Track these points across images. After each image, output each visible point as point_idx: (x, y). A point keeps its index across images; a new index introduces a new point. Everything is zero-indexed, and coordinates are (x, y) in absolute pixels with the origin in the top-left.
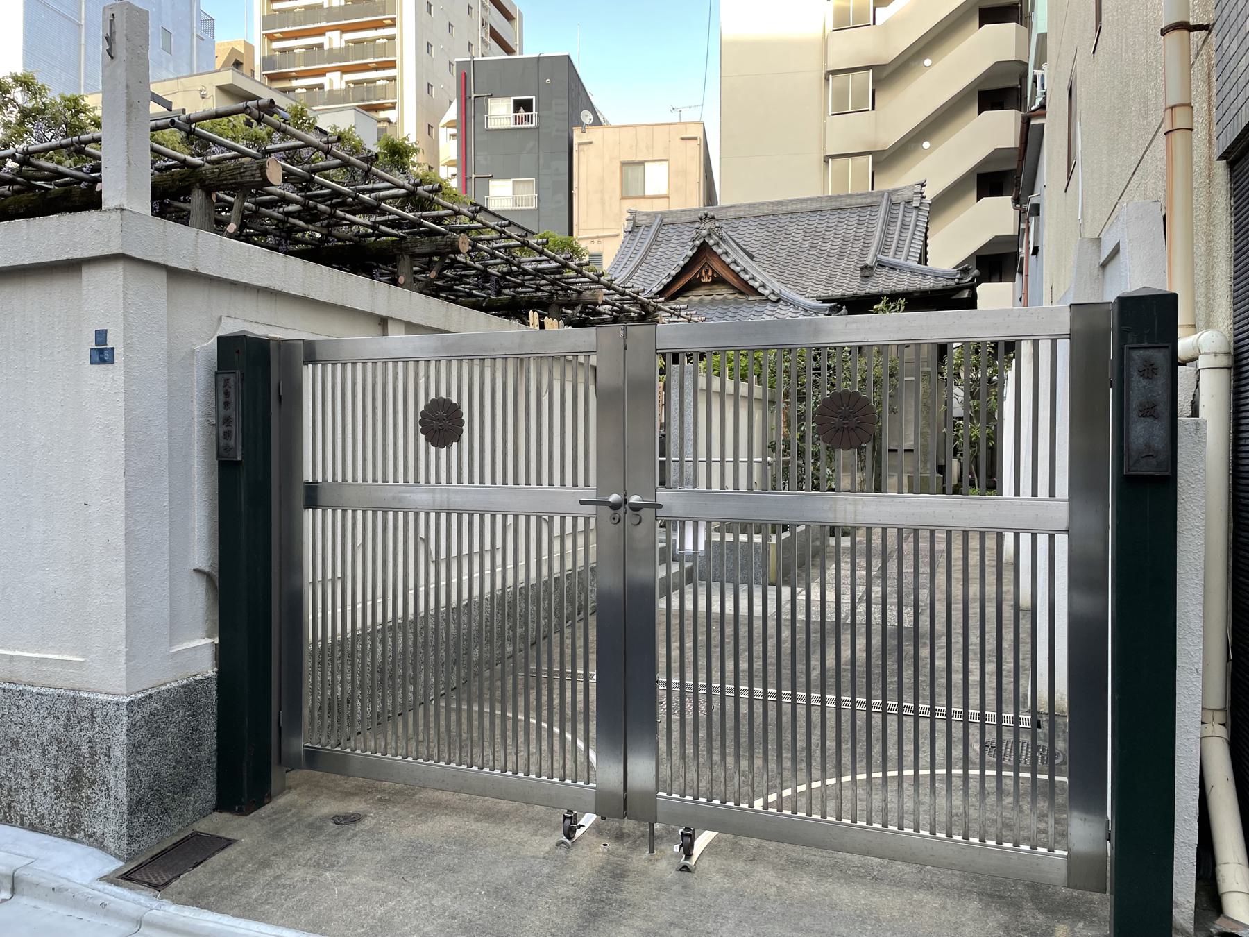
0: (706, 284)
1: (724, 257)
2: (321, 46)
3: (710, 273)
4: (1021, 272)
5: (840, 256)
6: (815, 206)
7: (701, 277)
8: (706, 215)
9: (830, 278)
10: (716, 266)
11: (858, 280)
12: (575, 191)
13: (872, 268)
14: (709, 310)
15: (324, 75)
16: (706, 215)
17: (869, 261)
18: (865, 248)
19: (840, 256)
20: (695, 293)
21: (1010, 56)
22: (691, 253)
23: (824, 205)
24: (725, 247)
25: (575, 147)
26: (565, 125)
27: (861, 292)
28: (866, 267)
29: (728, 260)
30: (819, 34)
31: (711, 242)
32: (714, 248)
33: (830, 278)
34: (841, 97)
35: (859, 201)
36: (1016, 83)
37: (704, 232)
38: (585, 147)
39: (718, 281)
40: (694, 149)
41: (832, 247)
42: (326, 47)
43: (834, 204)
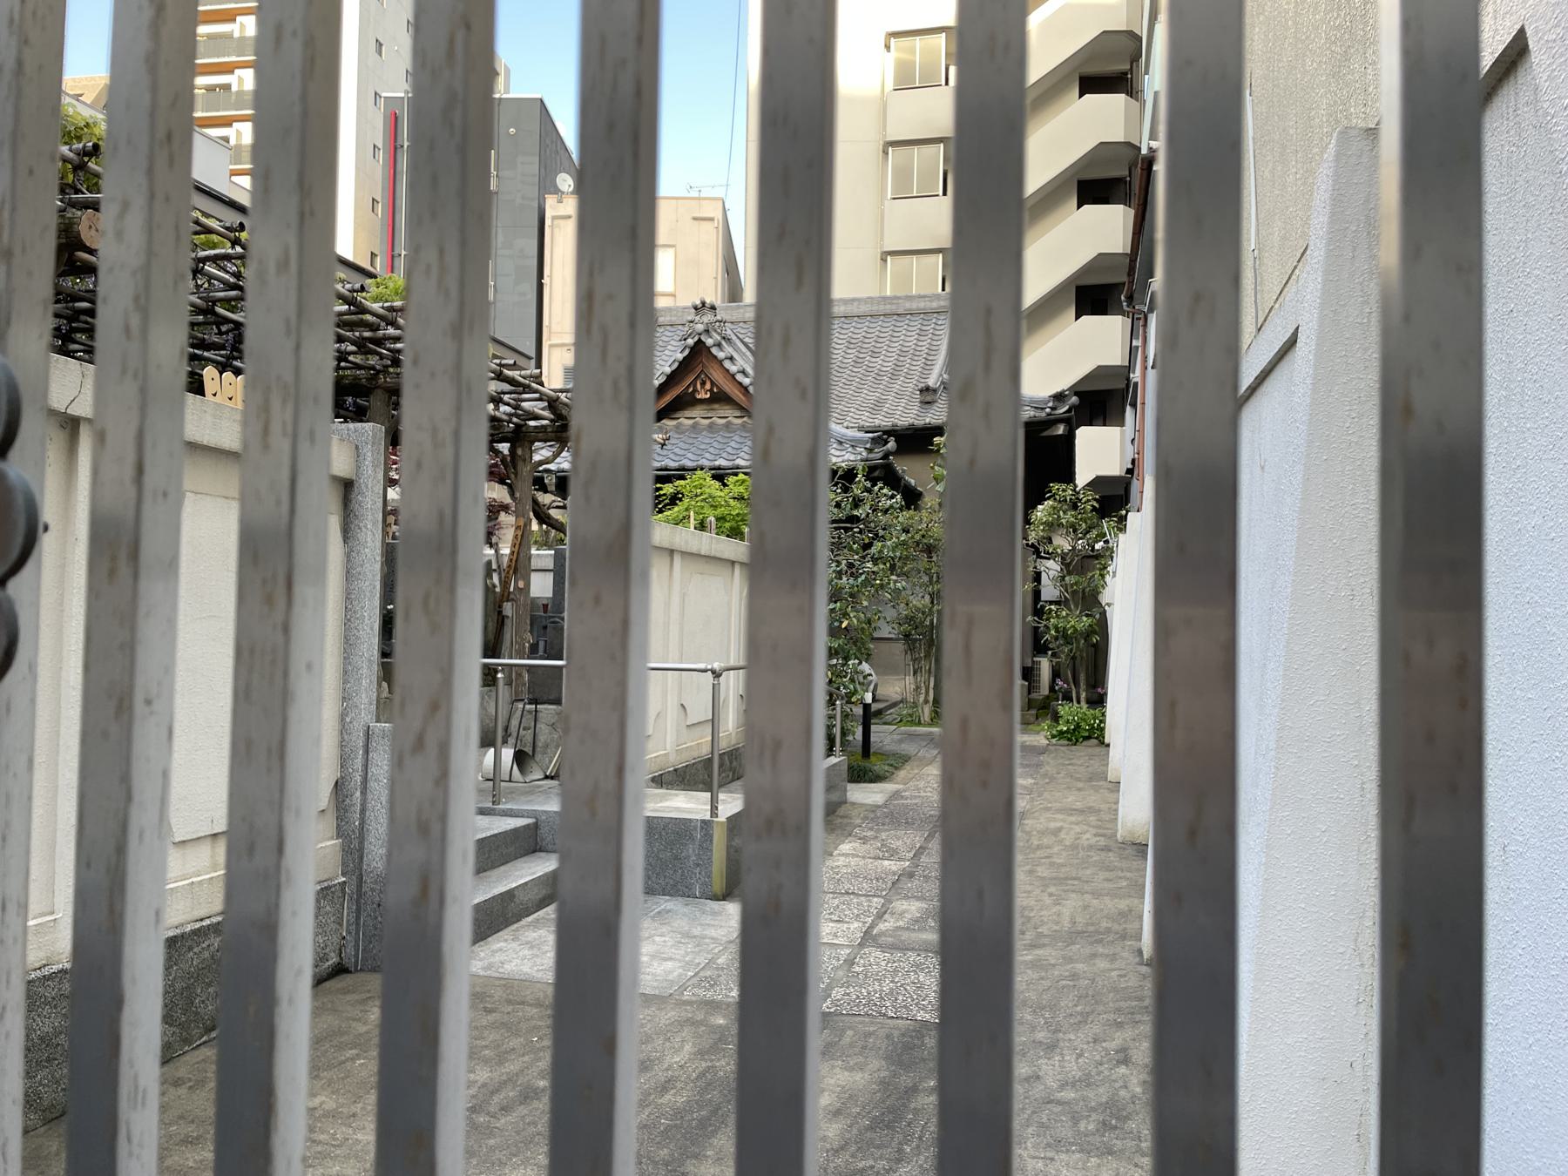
0: (702, 401)
1: (727, 364)
2: (227, 87)
3: (708, 386)
4: (1134, 405)
5: (894, 375)
6: (864, 309)
7: (695, 390)
8: (703, 304)
9: (879, 403)
10: (717, 375)
11: (916, 406)
12: (546, 281)
13: (935, 391)
14: (705, 438)
15: (230, 125)
16: (703, 304)
17: (932, 381)
18: (927, 366)
19: (894, 375)
20: (688, 413)
21: (1118, 136)
22: (680, 357)
23: (875, 309)
24: (729, 350)
25: (548, 222)
26: (533, 192)
27: (919, 423)
28: (927, 389)
29: (733, 369)
30: (877, 92)
31: (709, 342)
32: (714, 351)
33: (879, 403)
34: (903, 176)
35: (922, 305)
36: (1125, 279)
37: (700, 327)
38: (561, 222)
39: (719, 398)
40: (710, 237)
41: (884, 363)
42: (234, 88)
43: (888, 308)
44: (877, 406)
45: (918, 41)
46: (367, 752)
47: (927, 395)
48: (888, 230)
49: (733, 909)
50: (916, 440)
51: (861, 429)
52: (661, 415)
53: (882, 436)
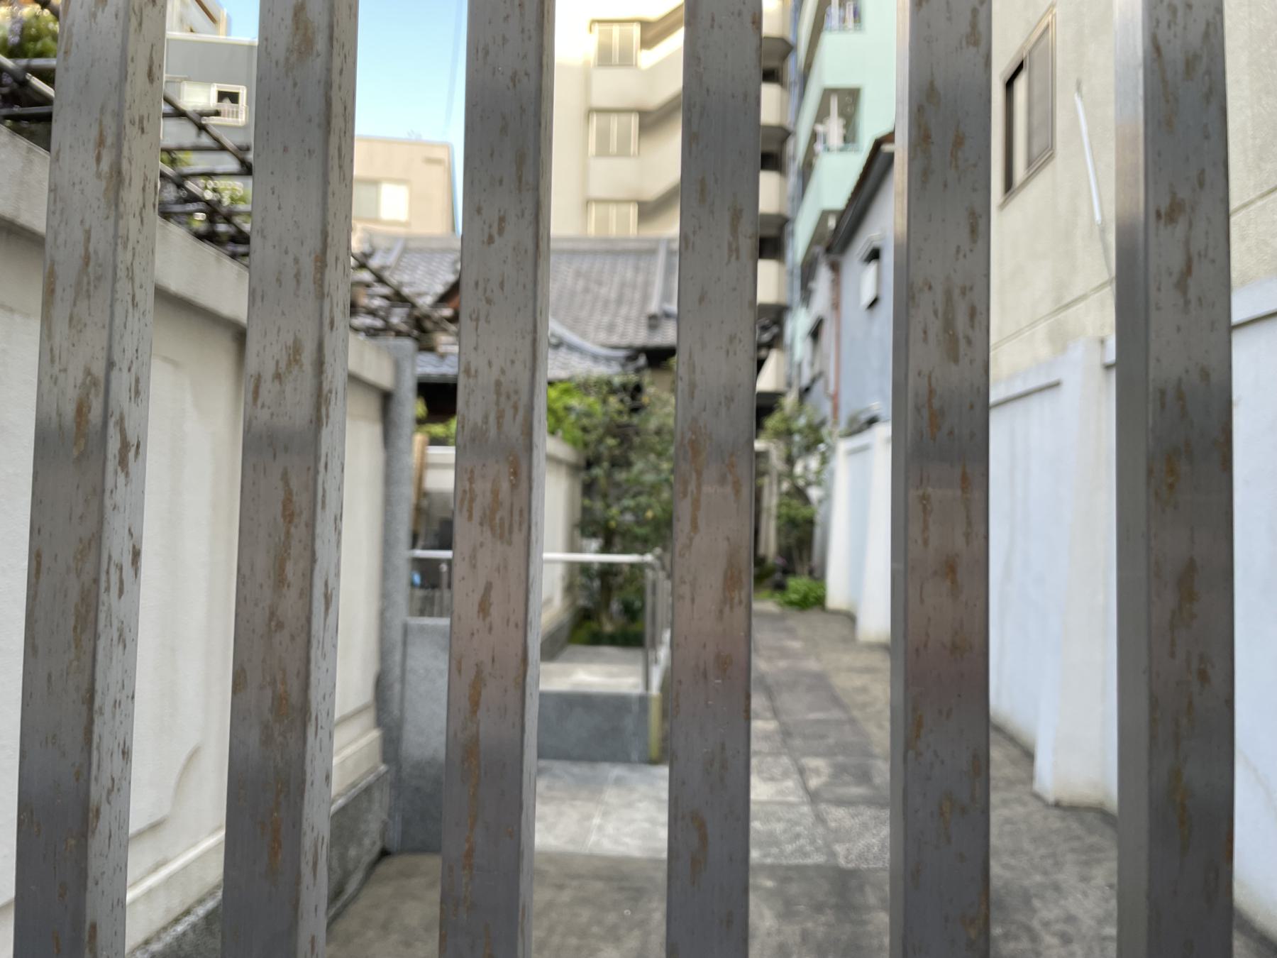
5: (619, 301)
18: (646, 298)
34: (603, 137)
44: (611, 328)
45: (616, 29)
46: (405, 644)
47: (654, 322)
48: (609, 179)
49: (664, 771)
50: (658, 358)
51: (604, 346)
52: (959, 247)
53: (634, 353)
